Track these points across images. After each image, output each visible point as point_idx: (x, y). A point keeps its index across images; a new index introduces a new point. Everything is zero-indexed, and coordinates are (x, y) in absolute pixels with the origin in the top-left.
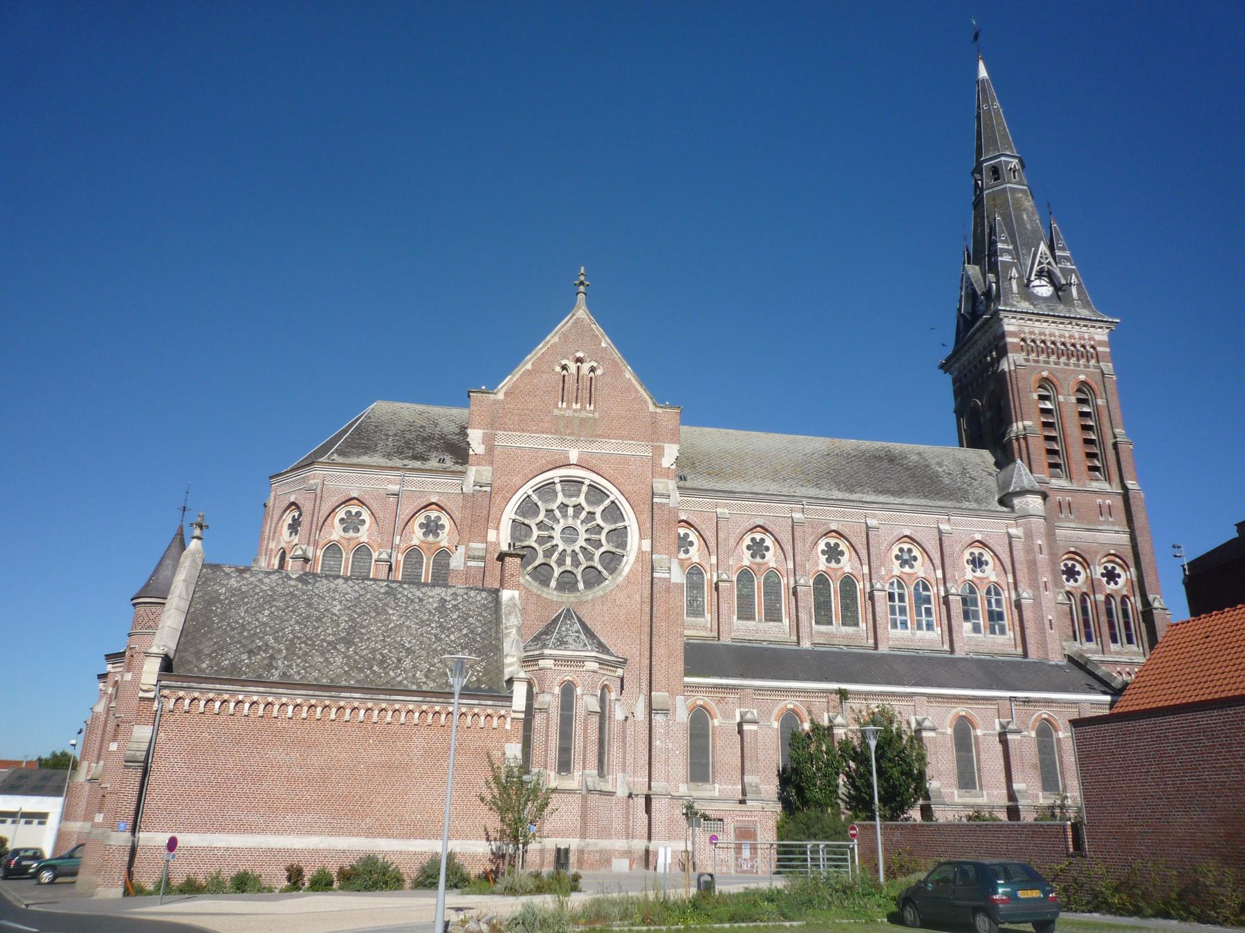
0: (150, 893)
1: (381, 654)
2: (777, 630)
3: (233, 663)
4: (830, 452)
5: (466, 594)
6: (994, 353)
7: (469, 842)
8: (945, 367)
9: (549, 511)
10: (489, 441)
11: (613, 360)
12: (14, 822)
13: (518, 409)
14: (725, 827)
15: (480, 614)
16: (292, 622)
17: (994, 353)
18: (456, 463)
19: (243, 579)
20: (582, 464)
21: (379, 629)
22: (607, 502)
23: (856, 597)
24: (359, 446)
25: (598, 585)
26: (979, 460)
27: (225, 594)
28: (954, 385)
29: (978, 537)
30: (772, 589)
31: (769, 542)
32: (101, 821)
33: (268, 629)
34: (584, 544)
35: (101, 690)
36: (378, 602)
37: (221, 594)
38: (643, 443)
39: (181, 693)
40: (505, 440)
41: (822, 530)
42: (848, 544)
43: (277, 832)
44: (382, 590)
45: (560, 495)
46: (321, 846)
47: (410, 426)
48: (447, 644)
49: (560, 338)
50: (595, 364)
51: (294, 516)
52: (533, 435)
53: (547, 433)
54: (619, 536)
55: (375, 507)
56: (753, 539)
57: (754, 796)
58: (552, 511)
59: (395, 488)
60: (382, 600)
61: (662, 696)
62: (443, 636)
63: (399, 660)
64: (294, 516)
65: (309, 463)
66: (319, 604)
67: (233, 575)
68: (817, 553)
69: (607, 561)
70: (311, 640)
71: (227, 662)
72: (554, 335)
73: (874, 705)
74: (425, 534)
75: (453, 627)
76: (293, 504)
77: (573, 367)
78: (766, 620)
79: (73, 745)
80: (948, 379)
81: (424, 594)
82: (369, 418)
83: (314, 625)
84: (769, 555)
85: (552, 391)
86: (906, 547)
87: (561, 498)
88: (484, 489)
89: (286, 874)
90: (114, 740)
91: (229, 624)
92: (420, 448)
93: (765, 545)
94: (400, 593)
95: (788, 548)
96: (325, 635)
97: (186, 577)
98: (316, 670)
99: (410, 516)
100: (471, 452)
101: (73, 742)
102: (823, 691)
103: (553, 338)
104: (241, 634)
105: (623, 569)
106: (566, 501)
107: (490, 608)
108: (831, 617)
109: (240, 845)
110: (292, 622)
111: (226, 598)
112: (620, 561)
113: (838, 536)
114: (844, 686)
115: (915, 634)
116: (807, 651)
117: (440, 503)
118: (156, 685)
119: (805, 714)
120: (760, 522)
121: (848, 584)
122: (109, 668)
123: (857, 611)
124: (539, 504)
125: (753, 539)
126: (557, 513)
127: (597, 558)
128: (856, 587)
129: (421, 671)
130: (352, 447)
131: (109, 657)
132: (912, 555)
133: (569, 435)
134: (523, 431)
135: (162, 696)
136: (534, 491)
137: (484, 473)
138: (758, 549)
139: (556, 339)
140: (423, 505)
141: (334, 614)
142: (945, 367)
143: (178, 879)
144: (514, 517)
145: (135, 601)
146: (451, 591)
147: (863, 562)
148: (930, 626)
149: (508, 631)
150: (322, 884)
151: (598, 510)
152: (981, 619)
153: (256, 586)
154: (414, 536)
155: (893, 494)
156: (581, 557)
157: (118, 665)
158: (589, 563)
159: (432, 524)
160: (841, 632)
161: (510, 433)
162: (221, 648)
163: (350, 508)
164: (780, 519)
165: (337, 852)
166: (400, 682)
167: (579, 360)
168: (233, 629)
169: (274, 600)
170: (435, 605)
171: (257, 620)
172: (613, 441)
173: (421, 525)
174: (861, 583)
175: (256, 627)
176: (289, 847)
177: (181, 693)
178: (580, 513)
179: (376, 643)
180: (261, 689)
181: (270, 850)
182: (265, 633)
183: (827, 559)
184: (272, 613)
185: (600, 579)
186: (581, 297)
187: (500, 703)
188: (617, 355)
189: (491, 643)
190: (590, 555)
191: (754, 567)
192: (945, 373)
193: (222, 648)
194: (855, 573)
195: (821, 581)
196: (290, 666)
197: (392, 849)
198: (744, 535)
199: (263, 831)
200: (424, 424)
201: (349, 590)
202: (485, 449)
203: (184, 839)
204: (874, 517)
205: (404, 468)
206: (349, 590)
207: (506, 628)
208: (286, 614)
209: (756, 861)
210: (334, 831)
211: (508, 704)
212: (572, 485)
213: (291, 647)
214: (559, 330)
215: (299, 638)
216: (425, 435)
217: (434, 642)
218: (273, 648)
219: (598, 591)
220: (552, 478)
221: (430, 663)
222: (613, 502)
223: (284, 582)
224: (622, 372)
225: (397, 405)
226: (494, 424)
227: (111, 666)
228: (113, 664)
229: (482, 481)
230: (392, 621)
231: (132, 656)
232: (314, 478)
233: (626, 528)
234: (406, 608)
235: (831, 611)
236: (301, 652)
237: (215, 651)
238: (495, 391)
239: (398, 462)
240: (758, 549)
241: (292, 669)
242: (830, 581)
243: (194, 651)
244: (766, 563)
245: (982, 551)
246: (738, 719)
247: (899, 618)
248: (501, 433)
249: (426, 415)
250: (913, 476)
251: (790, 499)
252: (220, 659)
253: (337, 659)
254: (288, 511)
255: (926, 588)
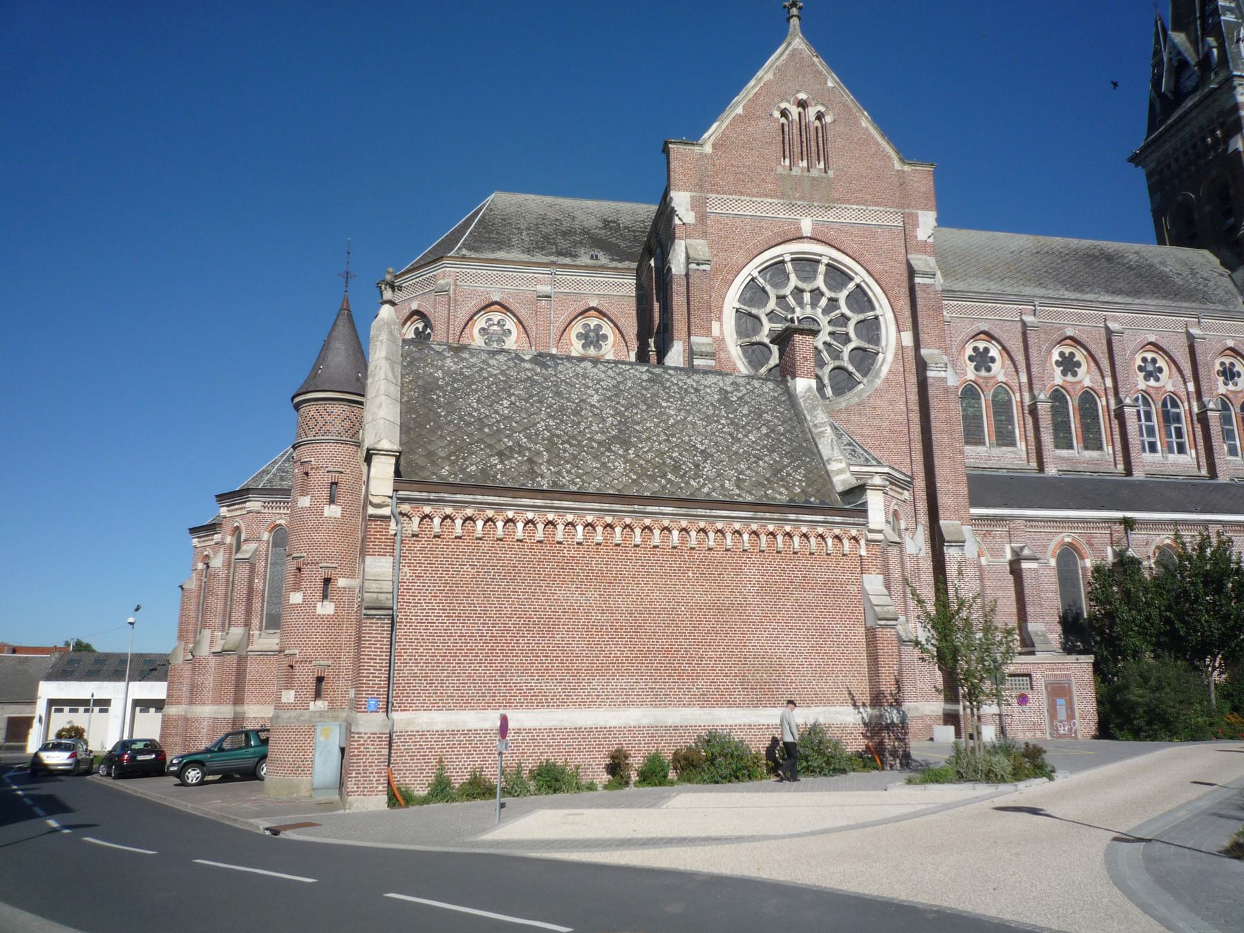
0: (424, 801)
1: (671, 458)
2: (1013, 455)
3: (482, 470)
4: (1039, 249)
5: (748, 383)
6: (1218, 132)
7: (833, 709)
8: (1135, 159)
9: (781, 298)
10: (699, 206)
11: (844, 104)
12: (86, 711)
13: (732, 166)
14: (1034, 683)
15: (775, 410)
16: (543, 416)
17: (1218, 132)
18: (613, 260)
19: (463, 359)
20: (818, 237)
21: (657, 426)
22: (851, 285)
23: (1098, 416)
24: (489, 240)
25: (850, 389)
26: (1202, 261)
27: (443, 379)
28: (1148, 179)
29: (1230, 343)
30: (1002, 408)
31: (994, 352)
32: (292, 700)
33: (514, 424)
34: (828, 339)
35: (195, 547)
36: (645, 392)
37: (438, 379)
38: (892, 210)
39: (427, 509)
40: (717, 205)
41: (1056, 336)
42: (1085, 353)
43: (583, 704)
44: (645, 377)
45: (793, 277)
46: (645, 722)
47: (543, 219)
48: (749, 445)
49: (775, 74)
50: (822, 109)
51: (417, 328)
52: (754, 199)
53: (771, 197)
54: (870, 329)
55: (522, 313)
56: (975, 349)
57: (1044, 647)
58: (784, 297)
59: (546, 289)
60: (648, 389)
61: (953, 525)
62: (740, 436)
63: (697, 466)
64: (417, 328)
65: (436, 257)
66: (570, 393)
67: (446, 354)
68: (1051, 365)
69: (858, 359)
70: (576, 440)
71: (474, 468)
72: (768, 71)
73: (1166, 538)
74: (584, 346)
75: (748, 423)
76: (416, 312)
77: (794, 111)
78: (999, 445)
79: (131, 623)
80: (1141, 173)
81: (698, 382)
82: (491, 210)
83: (573, 420)
84: (996, 367)
85: (772, 142)
86: (1149, 356)
87: (794, 281)
88: (702, 267)
89: (608, 761)
90: (297, 589)
91: (461, 418)
92: (563, 244)
93: (990, 355)
94: (667, 380)
95: (1020, 358)
96: (590, 433)
97: (388, 353)
98: (595, 478)
99: (566, 324)
100: (677, 221)
101: (131, 620)
102: (1105, 521)
103: (765, 74)
104: (480, 430)
105: (880, 370)
106: (801, 285)
107: (784, 401)
108: (1071, 440)
109: (537, 725)
110: (543, 416)
111: (447, 384)
112: (874, 361)
113: (1073, 343)
114: (1129, 514)
115: (1167, 458)
116: (1053, 478)
117: (601, 308)
118: (391, 497)
119: (1086, 549)
120: (985, 327)
121: (1088, 400)
122: (224, 511)
123: (1100, 432)
124: (768, 288)
125: (975, 349)
126: (791, 301)
127: (846, 355)
128: (1096, 404)
129: (729, 480)
130: (483, 242)
131: (222, 498)
132: (1157, 365)
133: (800, 200)
134: (741, 194)
135: (401, 514)
136: (759, 272)
137: (699, 248)
138: (982, 360)
139: (770, 76)
140: (580, 310)
141: (593, 406)
142: (1135, 159)
143: (459, 778)
144: (738, 305)
145: (296, 400)
146: (729, 380)
147: (1105, 373)
148: (1181, 449)
149: (819, 430)
150: (653, 775)
151: (842, 296)
152: (1238, 440)
153: (482, 369)
154: (572, 348)
155: (1128, 294)
156: (825, 355)
157: (237, 507)
158: (837, 363)
159: (592, 334)
160: (1085, 457)
161: (725, 197)
162: (461, 449)
163: (490, 315)
164: (1007, 323)
165: (667, 728)
166: (708, 494)
167: (802, 104)
168: (469, 424)
169: (510, 387)
170: (716, 397)
171: (496, 412)
172: (854, 207)
173: (579, 336)
174: (1104, 399)
175: (498, 422)
176: (602, 724)
177: (427, 509)
178: (819, 301)
179: (660, 444)
180: (539, 502)
181: (578, 730)
182: (513, 430)
183: (1062, 372)
184: (512, 403)
185: (850, 382)
186: (795, 22)
187: (851, 520)
188: (849, 98)
189: (801, 445)
190: (836, 354)
191: (980, 381)
192: (1136, 167)
193: (460, 450)
194: (1095, 387)
195: (1058, 397)
196: (559, 473)
197: (738, 722)
198: (967, 342)
199: (563, 704)
200: (559, 218)
201: (603, 376)
202: (696, 217)
203: (520, 719)
204: (1115, 319)
205: (553, 264)
206: (603, 376)
207: (815, 426)
208: (532, 405)
209: (1074, 724)
210: (659, 700)
211: (861, 520)
212: (806, 264)
213: (551, 446)
214: (773, 64)
215: (558, 436)
216: (565, 229)
217: (733, 444)
218: (529, 449)
219: (851, 398)
220: (782, 255)
221: (736, 470)
222: (858, 286)
223: (516, 365)
224: (857, 119)
225: (520, 197)
226: (703, 185)
227: (226, 508)
228: (228, 506)
229: (699, 257)
230: (670, 416)
231: (307, 474)
232: (444, 277)
233: (876, 318)
234: (682, 399)
235: (1071, 433)
236: (567, 454)
237: (453, 453)
238: (700, 142)
239: (540, 258)
240: (982, 360)
241: (563, 477)
242: (1068, 397)
243: (424, 453)
244: (994, 377)
245: (1233, 360)
246: (1009, 556)
247: (1146, 439)
248: (714, 196)
249: (557, 207)
250: (1140, 275)
251: (1018, 299)
252: (463, 464)
253: (616, 464)
254: (409, 323)
255: (1175, 405)
